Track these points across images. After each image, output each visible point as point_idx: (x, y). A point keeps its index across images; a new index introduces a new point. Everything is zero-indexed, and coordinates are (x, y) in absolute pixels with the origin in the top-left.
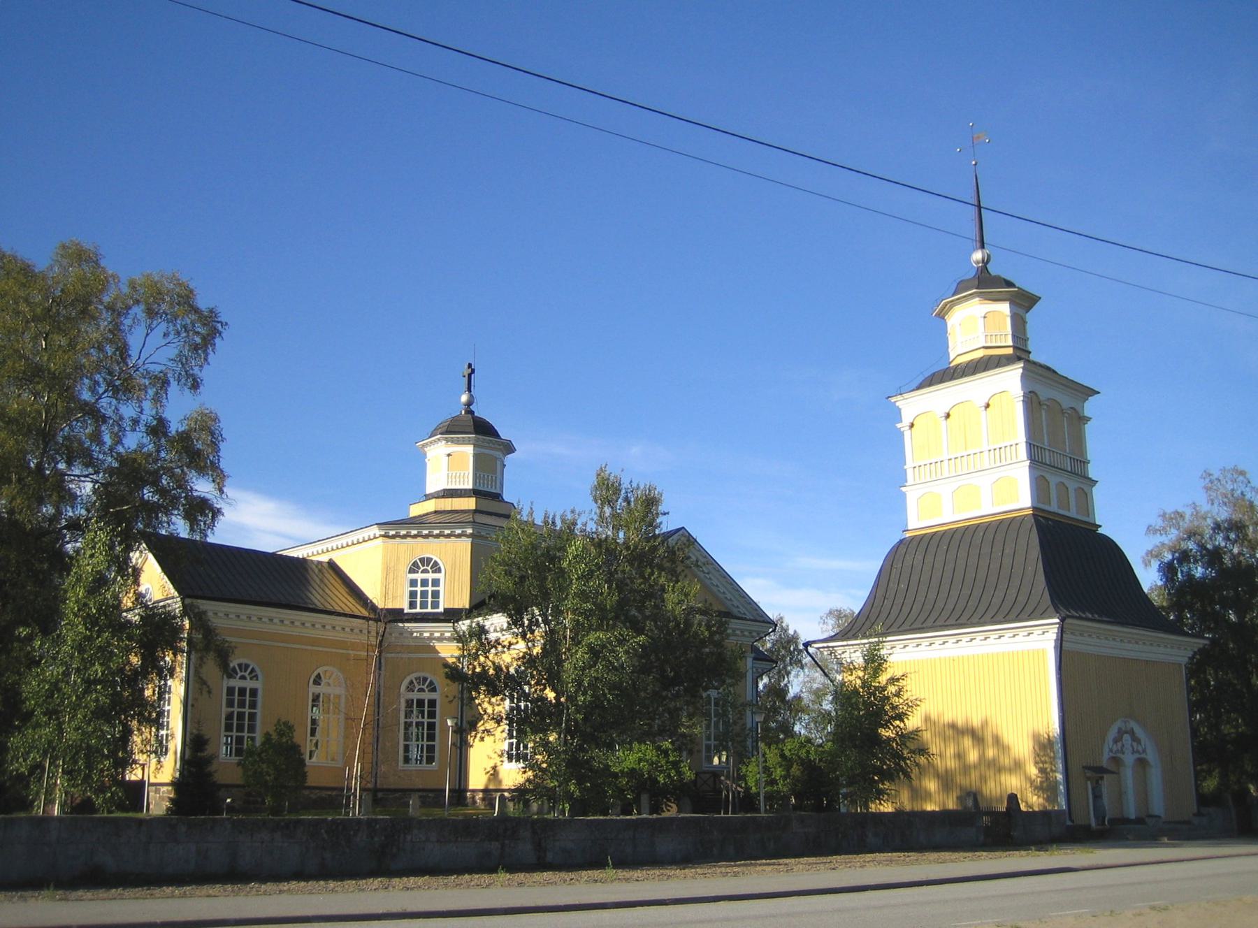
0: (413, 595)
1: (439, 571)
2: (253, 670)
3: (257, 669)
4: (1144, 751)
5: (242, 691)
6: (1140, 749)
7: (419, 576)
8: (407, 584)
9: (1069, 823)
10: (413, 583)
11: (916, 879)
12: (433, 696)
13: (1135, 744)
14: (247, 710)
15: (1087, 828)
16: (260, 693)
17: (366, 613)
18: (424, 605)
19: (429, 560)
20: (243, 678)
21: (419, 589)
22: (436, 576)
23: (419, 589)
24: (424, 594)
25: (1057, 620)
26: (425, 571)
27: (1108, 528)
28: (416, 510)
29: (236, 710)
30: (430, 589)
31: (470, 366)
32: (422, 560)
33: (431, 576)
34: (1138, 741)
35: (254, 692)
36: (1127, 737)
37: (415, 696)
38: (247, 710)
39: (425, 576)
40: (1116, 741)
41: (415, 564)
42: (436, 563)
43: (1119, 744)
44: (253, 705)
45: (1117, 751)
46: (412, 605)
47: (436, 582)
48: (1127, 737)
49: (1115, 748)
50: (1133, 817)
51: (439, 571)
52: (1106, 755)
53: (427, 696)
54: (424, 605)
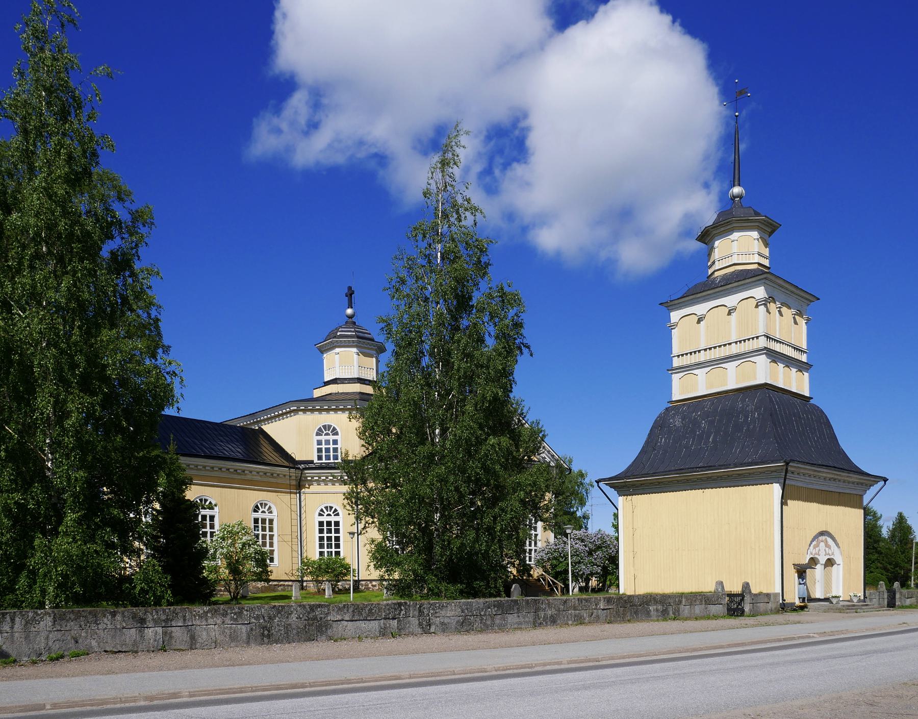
0: (320, 450)
1: (337, 434)
2: (336, 510)
3: (272, 506)
7: (323, 438)
8: (316, 443)
10: (319, 443)
11: (157, 714)
12: (336, 519)
14: (333, 535)
16: (275, 523)
17: (286, 464)
18: (328, 458)
19: (330, 426)
21: (324, 446)
22: (335, 437)
23: (324, 446)
24: (327, 450)
26: (327, 434)
28: (317, 393)
29: (325, 535)
30: (331, 446)
31: (350, 288)
32: (324, 427)
33: (331, 438)
34: (829, 547)
35: (337, 524)
36: (822, 544)
37: (325, 519)
38: (268, 533)
39: (327, 437)
41: (320, 429)
42: (334, 429)
44: (337, 531)
46: (320, 458)
47: (335, 442)
48: (822, 544)
51: (337, 434)
53: (333, 519)
54: (328, 458)
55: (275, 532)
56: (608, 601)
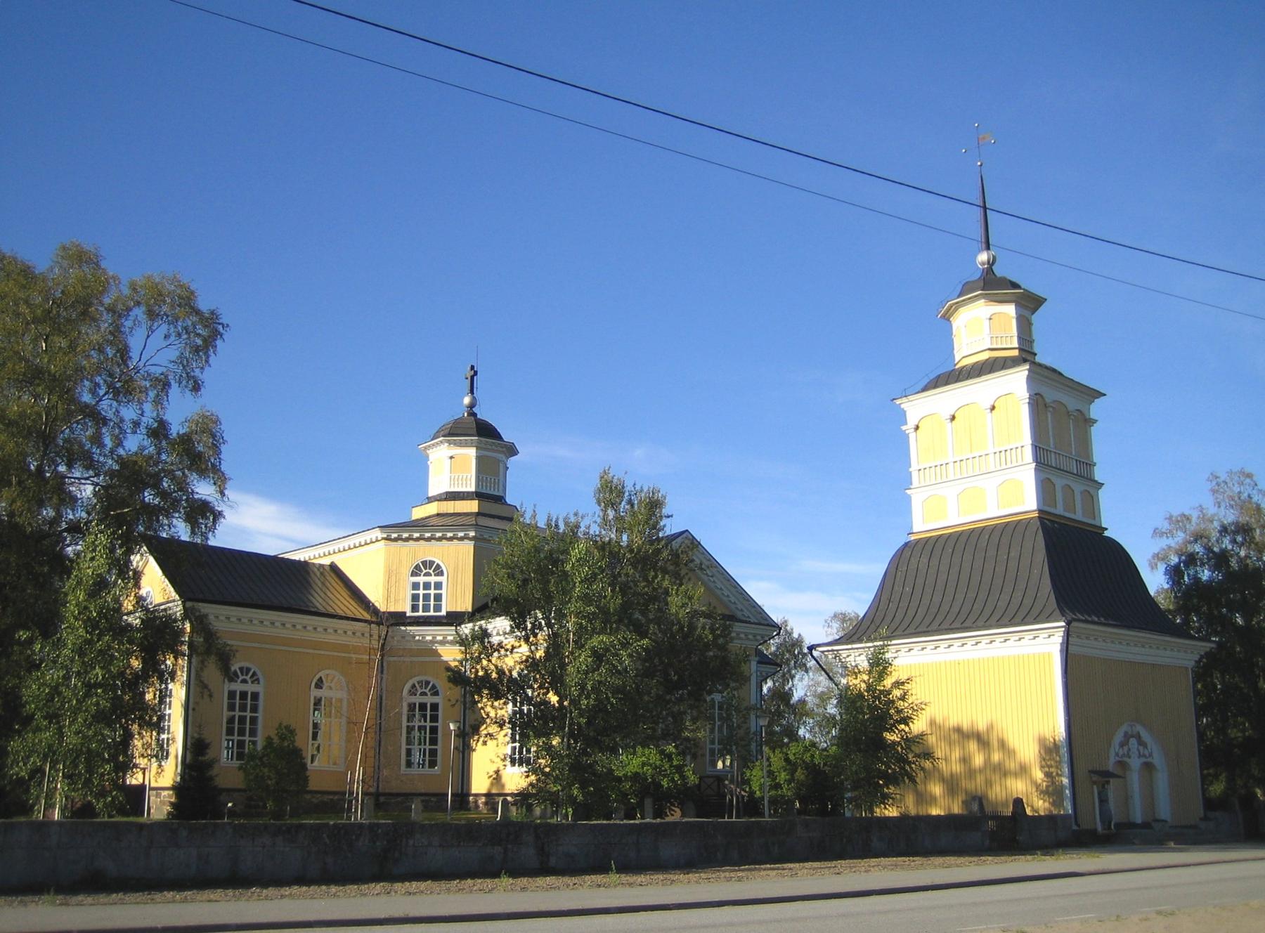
0: (415, 598)
1: (441, 574)
2: (254, 674)
3: (259, 673)
4: (1151, 755)
5: (244, 695)
6: (1146, 753)
7: (421, 579)
8: (409, 587)
9: (1075, 827)
10: (415, 586)
12: (435, 699)
13: (1141, 748)
14: (248, 714)
15: (1094, 832)
17: (368, 617)
18: (426, 608)
19: (432, 563)
20: (244, 681)
21: (421, 592)
22: (438, 579)
23: (421, 592)
24: (427, 597)
25: (1063, 624)
26: (427, 574)
27: (1114, 531)
28: (418, 513)
29: (237, 713)
30: (432, 592)
31: (472, 367)
32: (424, 563)
33: (433, 579)
34: (1144, 745)
35: (255, 696)
36: (1133, 741)
37: (418, 699)
38: (248, 714)
39: (427, 579)
40: (1122, 745)
41: (417, 567)
42: (438, 566)
43: (1126, 748)
44: (255, 709)
45: (1124, 755)
46: (415, 608)
47: (438, 586)
48: (1133, 741)
49: (1121, 752)
50: (1139, 821)
51: (441, 574)
52: (1112, 760)
53: (429, 700)
54: (426, 608)
55: (260, 715)
56: (378, 806)
